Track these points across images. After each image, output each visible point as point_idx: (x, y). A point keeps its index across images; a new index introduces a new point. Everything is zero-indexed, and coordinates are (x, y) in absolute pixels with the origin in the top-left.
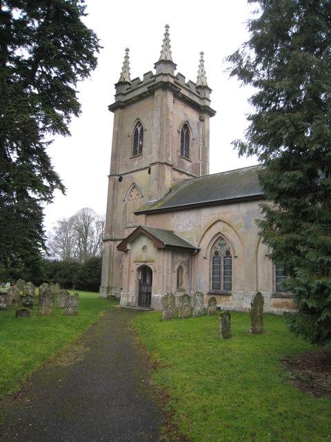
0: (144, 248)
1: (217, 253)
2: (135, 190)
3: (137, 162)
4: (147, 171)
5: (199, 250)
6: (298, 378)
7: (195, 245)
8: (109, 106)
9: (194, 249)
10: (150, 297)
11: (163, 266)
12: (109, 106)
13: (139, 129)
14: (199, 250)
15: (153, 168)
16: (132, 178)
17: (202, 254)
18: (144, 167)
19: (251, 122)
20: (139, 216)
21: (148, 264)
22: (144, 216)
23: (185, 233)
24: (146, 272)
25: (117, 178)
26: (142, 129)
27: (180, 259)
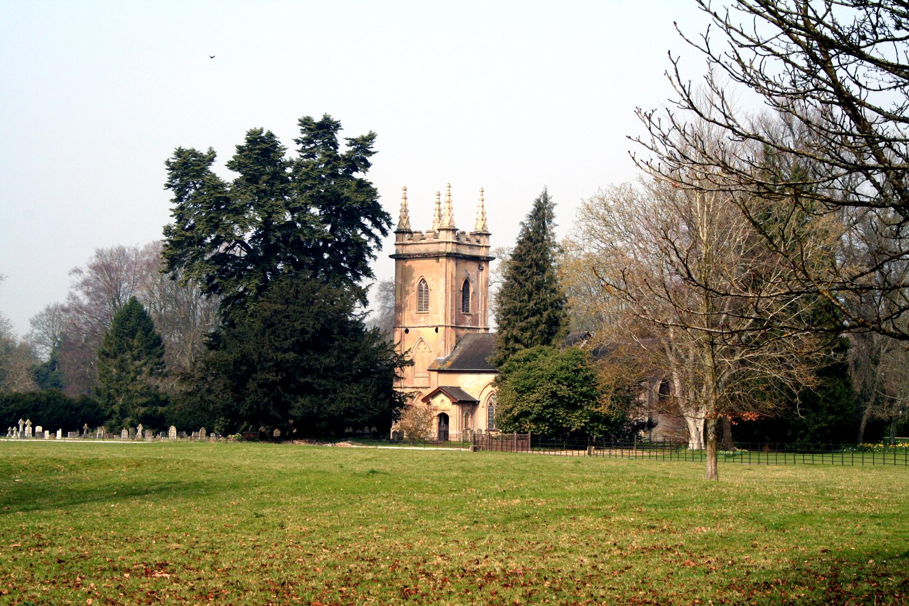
0: (442, 401)
1: (491, 404)
2: (422, 343)
3: (423, 318)
4: (435, 328)
5: (479, 402)
6: (857, 194)
7: (477, 399)
8: (180, 153)
9: (476, 401)
10: (448, 435)
11: (454, 412)
12: (180, 153)
13: (424, 285)
14: (479, 402)
15: (439, 329)
16: (419, 333)
17: (481, 405)
18: (430, 325)
19: (498, 291)
20: (432, 373)
21: (445, 412)
22: (436, 373)
23: (469, 389)
24: (444, 418)
25: (404, 329)
26: (427, 286)
27: (467, 408)
